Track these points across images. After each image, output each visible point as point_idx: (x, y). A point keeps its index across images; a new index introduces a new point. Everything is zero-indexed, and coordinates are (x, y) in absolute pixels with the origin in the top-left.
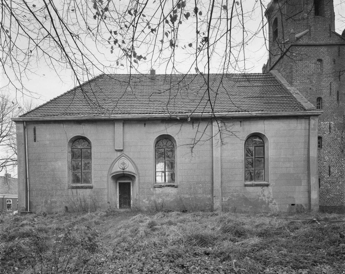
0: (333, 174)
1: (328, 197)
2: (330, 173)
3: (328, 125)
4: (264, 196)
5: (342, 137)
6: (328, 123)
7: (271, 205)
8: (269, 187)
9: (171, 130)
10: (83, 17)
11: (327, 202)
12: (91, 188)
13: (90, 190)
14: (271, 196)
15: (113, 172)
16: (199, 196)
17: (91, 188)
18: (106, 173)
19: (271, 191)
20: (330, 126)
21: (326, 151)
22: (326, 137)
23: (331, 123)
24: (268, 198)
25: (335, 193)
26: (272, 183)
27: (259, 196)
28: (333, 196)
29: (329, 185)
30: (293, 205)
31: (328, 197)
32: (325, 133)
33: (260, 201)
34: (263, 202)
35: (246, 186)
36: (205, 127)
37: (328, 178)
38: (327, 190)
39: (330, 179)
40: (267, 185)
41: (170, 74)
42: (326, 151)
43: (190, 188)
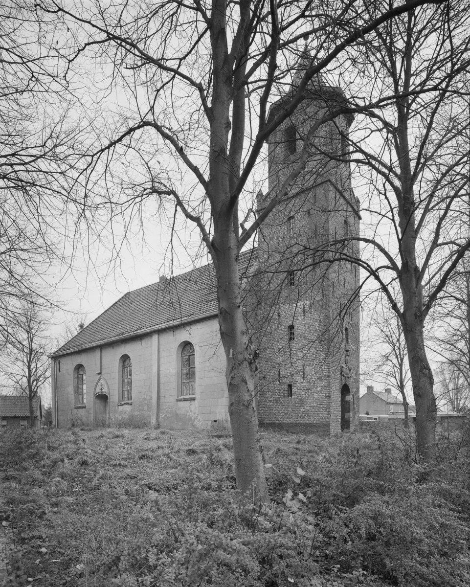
0: (308, 377)
1: (302, 410)
2: (304, 376)
3: (302, 307)
4: (191, 411)
5: (320, 321)
6: (302, 303)
7: (196, 421)
8: (196, 401)
9: (183, 336)
10: (192, 189)
11: (300, 417)
12: (84, 407)
13: (84, 409)
14: (197, 411)
15: (96, 392)
16: (145, 413)
17: (84, 407)
18: (92, 394)
19: (197, 406)
20: (304, 308)
21: (300, 345)
22: (299, 327)
23: (306, 302)
24: (194, 414)
25: (312, 405)
26: (197, 396)
27: (188, 412)
28: (308, 408)
29: (303, 393)
30: (215, 421)
31: (302, 410)
32: (298, 319)
33: (187, 417)
34: (190, 419)
35: (178, 401)
36: (99, 357)
37: (302, 383)
38: (301, 400)
39: (305, 384)
40: (193, 399)
41: (207, 264)
42: (300, 345)
43: (140, 405)
